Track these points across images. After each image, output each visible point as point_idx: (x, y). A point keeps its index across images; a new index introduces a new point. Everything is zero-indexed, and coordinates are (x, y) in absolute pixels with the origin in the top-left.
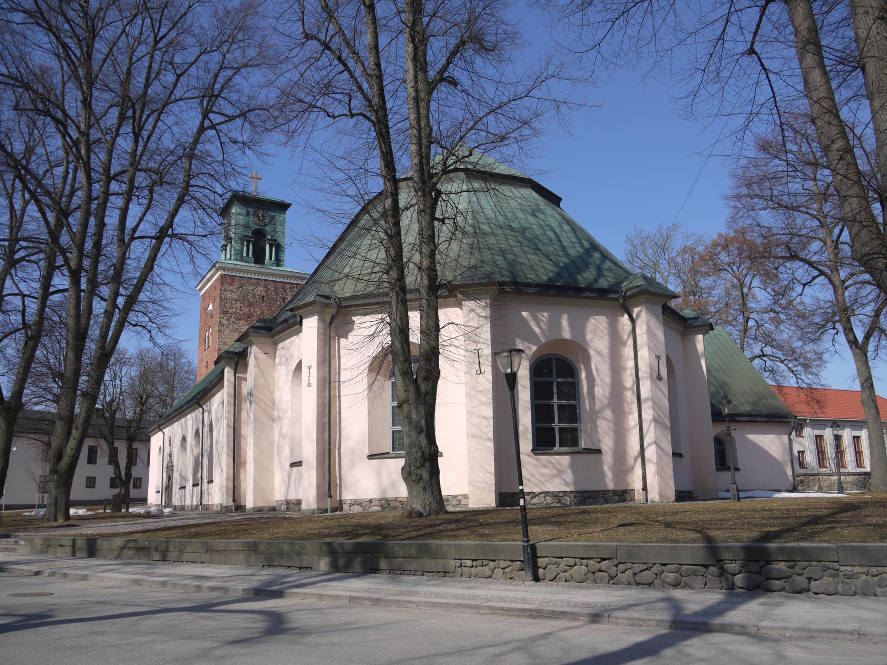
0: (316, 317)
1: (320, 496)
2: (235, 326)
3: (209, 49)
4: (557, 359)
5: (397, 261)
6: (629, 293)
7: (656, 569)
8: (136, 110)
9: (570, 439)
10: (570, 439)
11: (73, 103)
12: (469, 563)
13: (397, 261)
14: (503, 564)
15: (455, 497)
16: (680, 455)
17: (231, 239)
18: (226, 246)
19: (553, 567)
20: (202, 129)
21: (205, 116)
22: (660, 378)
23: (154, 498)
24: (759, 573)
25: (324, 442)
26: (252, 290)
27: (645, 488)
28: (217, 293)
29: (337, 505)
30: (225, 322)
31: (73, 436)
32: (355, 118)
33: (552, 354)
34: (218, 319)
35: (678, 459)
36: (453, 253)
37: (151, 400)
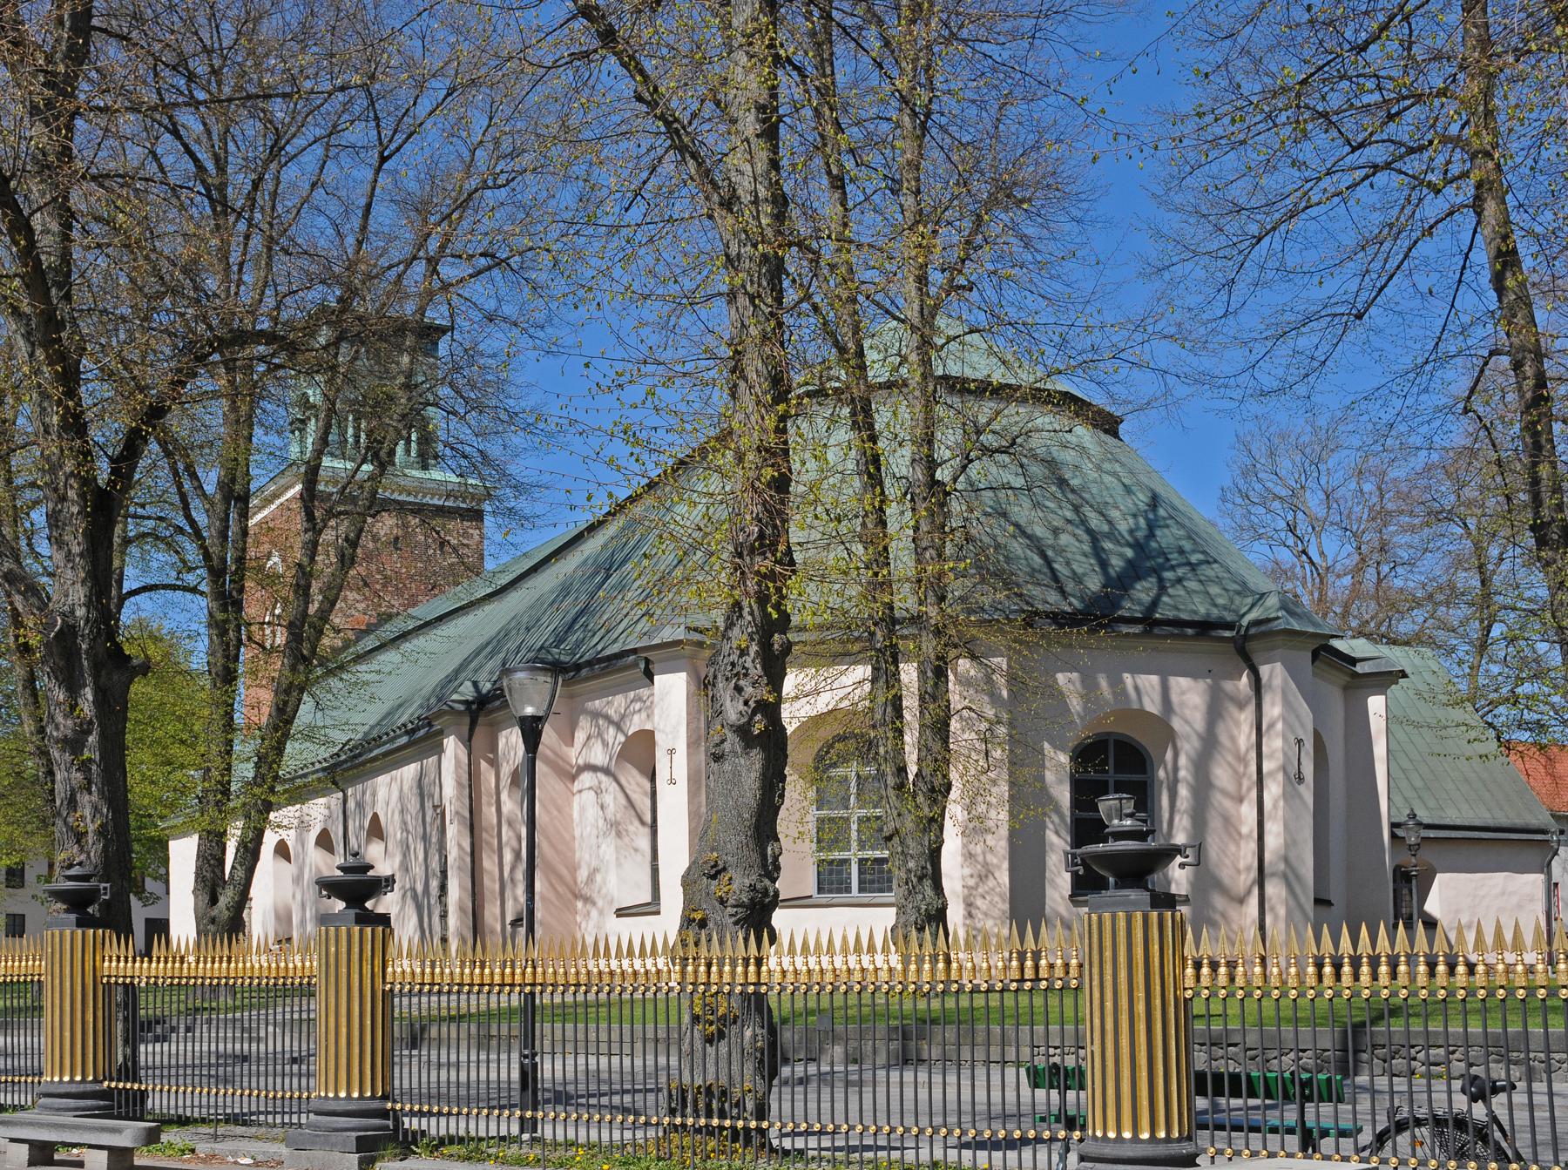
0: (683, 675)
4: (1117, 742)
6: (1253, 631)
9: (1139, 870)
10: (1139, 870)
11: (393, 273)
16: (1328, 903)
33: (1108, 734)
35: (1323, 909)
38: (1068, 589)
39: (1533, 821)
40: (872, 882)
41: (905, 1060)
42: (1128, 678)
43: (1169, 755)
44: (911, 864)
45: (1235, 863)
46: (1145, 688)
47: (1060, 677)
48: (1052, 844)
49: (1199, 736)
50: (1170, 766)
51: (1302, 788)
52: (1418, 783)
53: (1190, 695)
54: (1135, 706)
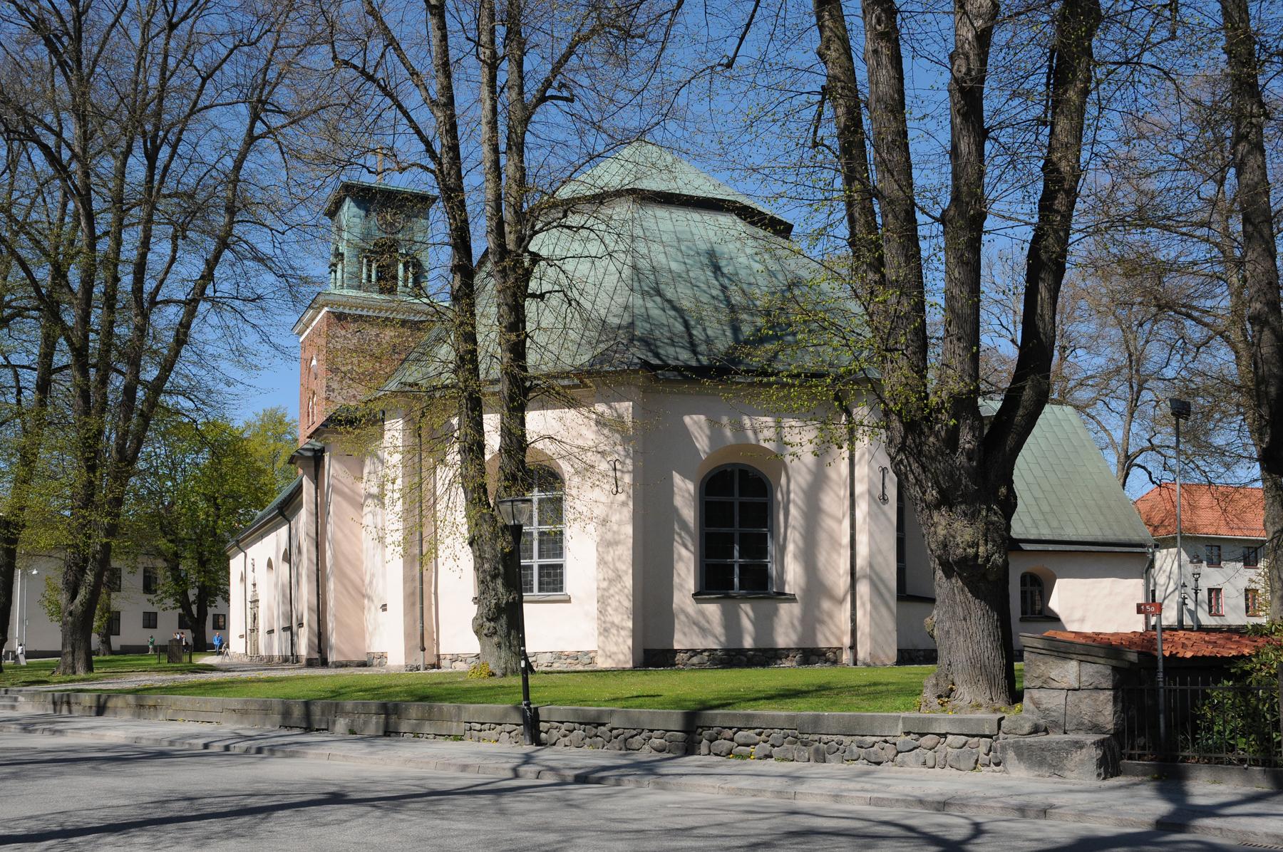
1: (408, 652)
2: (352, 392)
3: (245, 41)
5: (468, 361)
7: (645, 734)
8: (152, 129)
12: (478, 727)
13: (468, 361)
14: (509, 728)
15: (587, 653)
17: (342, 255)
18: (335, 265)
19: (555, 732)
20: (251, 139)
21: (255, 117)
22: (884, 499)
23: (237, 646)
24: (732, 740)
25: (413, 580)
26: (377, 335)
27: (853, 647)
28: (322, 341)
29: (434, 660)
30: (335, 385)
31: (151, 543)
32: (406, 174)
34: (324, 381)
36: (554, 341)
37: (691, 274)
38: (699, 349)
39: (1136, 538)
40: (548, 583)
41: (389, 732)
42: (746, 421)
43: (783, 480)
44: (486, 566)
45: (837, 572)
46: (761, 429)
47: (687, 419)
48: (679, 555)
49: (810, 470)
50: (785, 489)
51: (886, 507)
52: (1046, 508)
53: (802, 437)
54: (754, 442)
